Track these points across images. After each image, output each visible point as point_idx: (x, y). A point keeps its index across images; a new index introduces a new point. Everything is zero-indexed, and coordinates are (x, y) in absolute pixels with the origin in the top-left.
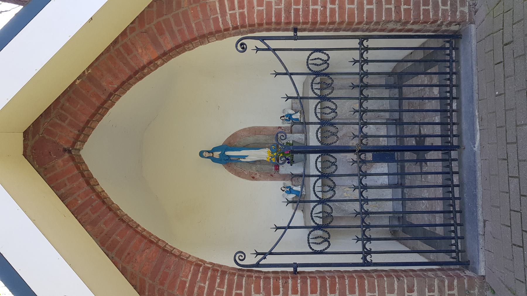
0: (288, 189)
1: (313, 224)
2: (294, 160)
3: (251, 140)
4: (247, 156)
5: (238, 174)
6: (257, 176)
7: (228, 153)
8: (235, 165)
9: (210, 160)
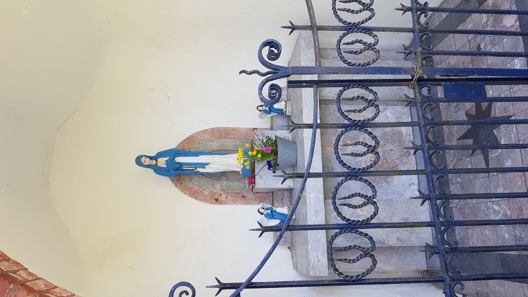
0: (269, 212)
1: (340, 221)
2: (278, 162)
3: (215, 145)
5: (194, 195)
6: (223, 198)
7: (179, 159)
8: (191, 181)
9: (151, 171)
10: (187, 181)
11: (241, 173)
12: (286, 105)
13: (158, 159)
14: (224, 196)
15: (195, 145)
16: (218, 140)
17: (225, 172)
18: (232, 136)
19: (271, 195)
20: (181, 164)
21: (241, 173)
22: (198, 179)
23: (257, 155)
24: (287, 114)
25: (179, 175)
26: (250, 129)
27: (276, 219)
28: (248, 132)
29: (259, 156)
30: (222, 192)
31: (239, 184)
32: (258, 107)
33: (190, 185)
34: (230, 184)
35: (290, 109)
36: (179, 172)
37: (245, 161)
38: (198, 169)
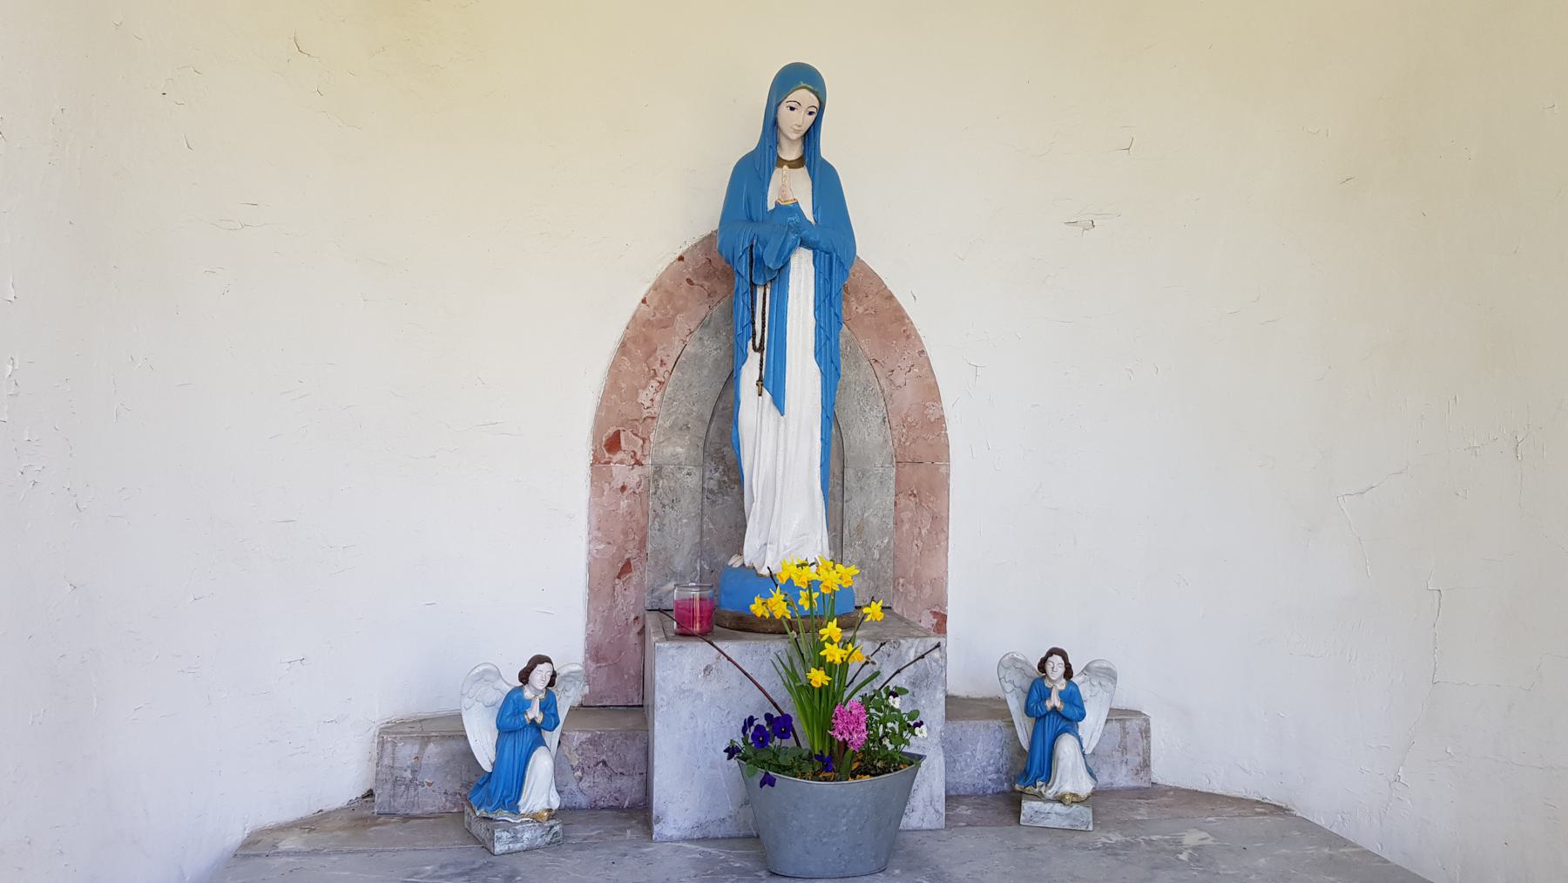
0: (534, 713)
3: (868, 435)
4: (779, 402)
5: (640, 342)
6: (622, 472)
7: (802, 269)
8: (703, 324)
9: (749, 139)
10: (703, 311)
11: (735, 562)
12: (1077, 800)
13: (803, 171)
14: (633, 477)
15: (866, 346)
16: (890, 448)
17: (740, 482)
18: (906, 515)
19: (623, 705)
20: (779, 276)
21: (735, 562)
22: (709, 361)
23: (821, 663)
24: (1028, 806)
25: (729, 274)
26: (942, 602)
27: (499, 747)
28: (927, 590)
29: (818, 678)
30: (649, 469)
31: (687, 547)
32: (1063, 654)
33: (683, 324)
34: (688, 505)
35: (1052, 822)
36: (743, 267)
37: (790, 589)
38: (754, 359)
